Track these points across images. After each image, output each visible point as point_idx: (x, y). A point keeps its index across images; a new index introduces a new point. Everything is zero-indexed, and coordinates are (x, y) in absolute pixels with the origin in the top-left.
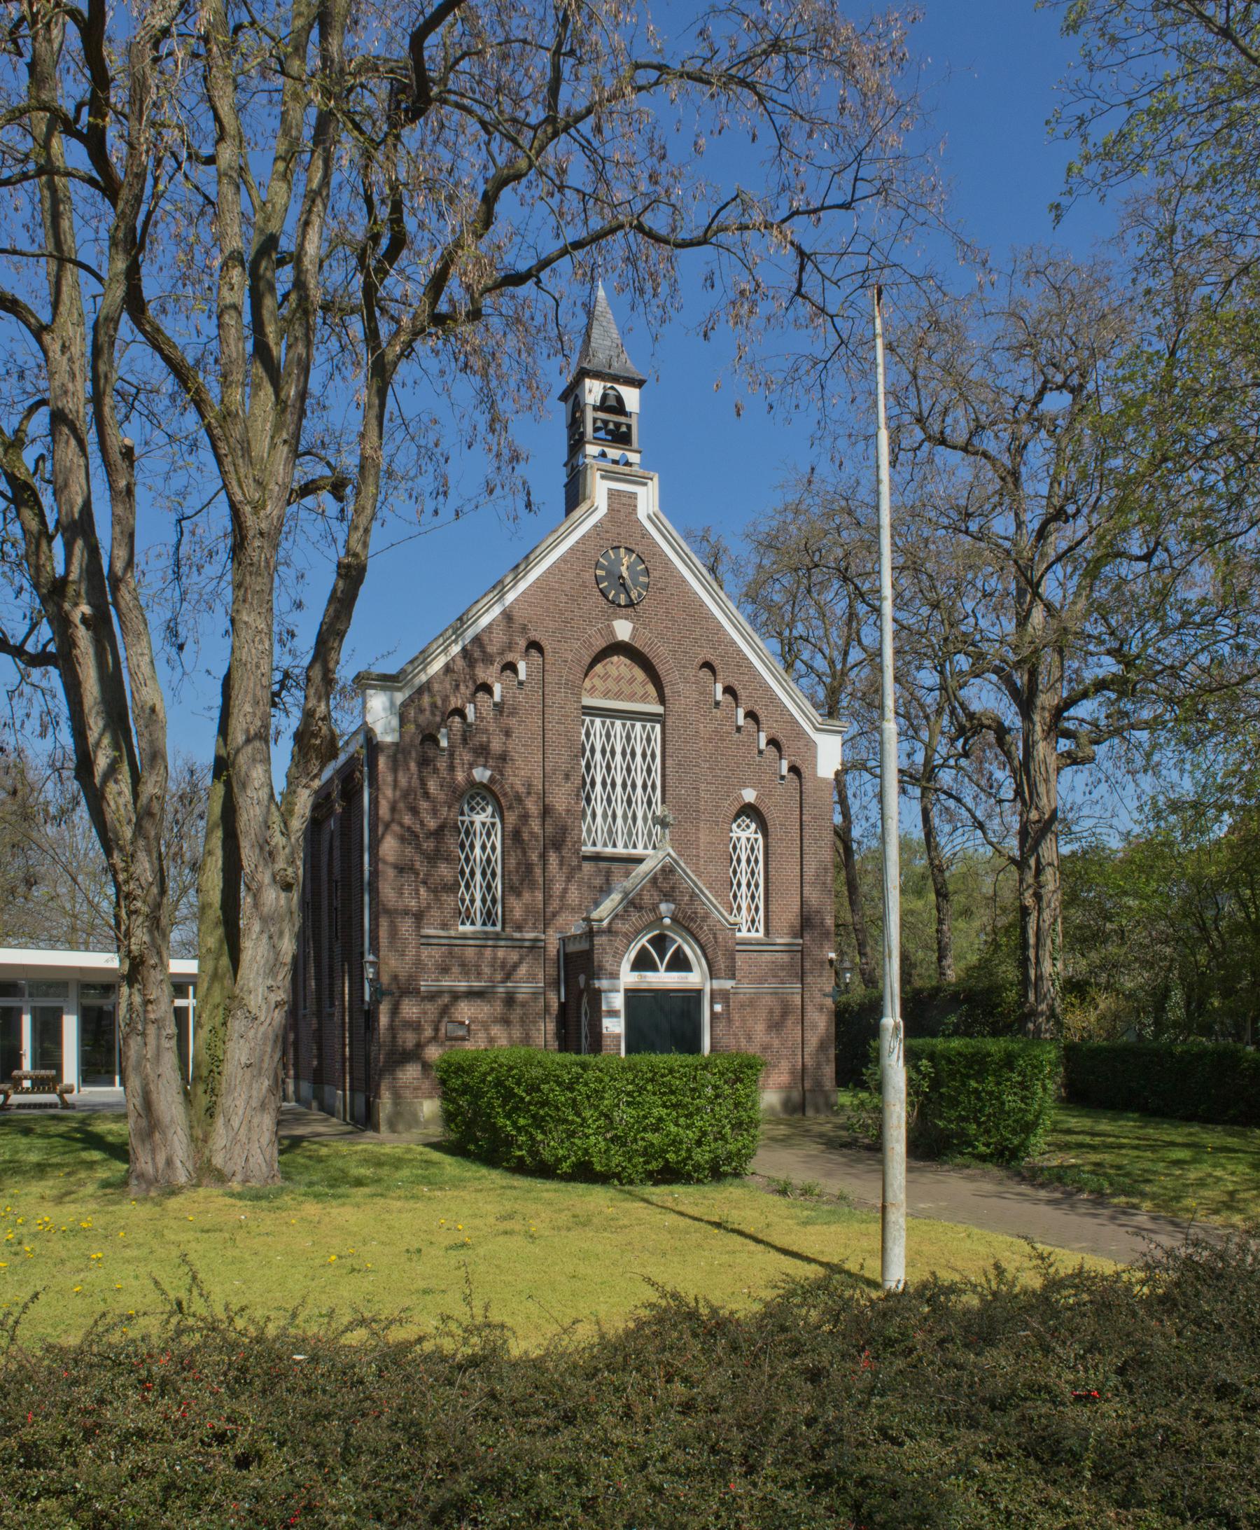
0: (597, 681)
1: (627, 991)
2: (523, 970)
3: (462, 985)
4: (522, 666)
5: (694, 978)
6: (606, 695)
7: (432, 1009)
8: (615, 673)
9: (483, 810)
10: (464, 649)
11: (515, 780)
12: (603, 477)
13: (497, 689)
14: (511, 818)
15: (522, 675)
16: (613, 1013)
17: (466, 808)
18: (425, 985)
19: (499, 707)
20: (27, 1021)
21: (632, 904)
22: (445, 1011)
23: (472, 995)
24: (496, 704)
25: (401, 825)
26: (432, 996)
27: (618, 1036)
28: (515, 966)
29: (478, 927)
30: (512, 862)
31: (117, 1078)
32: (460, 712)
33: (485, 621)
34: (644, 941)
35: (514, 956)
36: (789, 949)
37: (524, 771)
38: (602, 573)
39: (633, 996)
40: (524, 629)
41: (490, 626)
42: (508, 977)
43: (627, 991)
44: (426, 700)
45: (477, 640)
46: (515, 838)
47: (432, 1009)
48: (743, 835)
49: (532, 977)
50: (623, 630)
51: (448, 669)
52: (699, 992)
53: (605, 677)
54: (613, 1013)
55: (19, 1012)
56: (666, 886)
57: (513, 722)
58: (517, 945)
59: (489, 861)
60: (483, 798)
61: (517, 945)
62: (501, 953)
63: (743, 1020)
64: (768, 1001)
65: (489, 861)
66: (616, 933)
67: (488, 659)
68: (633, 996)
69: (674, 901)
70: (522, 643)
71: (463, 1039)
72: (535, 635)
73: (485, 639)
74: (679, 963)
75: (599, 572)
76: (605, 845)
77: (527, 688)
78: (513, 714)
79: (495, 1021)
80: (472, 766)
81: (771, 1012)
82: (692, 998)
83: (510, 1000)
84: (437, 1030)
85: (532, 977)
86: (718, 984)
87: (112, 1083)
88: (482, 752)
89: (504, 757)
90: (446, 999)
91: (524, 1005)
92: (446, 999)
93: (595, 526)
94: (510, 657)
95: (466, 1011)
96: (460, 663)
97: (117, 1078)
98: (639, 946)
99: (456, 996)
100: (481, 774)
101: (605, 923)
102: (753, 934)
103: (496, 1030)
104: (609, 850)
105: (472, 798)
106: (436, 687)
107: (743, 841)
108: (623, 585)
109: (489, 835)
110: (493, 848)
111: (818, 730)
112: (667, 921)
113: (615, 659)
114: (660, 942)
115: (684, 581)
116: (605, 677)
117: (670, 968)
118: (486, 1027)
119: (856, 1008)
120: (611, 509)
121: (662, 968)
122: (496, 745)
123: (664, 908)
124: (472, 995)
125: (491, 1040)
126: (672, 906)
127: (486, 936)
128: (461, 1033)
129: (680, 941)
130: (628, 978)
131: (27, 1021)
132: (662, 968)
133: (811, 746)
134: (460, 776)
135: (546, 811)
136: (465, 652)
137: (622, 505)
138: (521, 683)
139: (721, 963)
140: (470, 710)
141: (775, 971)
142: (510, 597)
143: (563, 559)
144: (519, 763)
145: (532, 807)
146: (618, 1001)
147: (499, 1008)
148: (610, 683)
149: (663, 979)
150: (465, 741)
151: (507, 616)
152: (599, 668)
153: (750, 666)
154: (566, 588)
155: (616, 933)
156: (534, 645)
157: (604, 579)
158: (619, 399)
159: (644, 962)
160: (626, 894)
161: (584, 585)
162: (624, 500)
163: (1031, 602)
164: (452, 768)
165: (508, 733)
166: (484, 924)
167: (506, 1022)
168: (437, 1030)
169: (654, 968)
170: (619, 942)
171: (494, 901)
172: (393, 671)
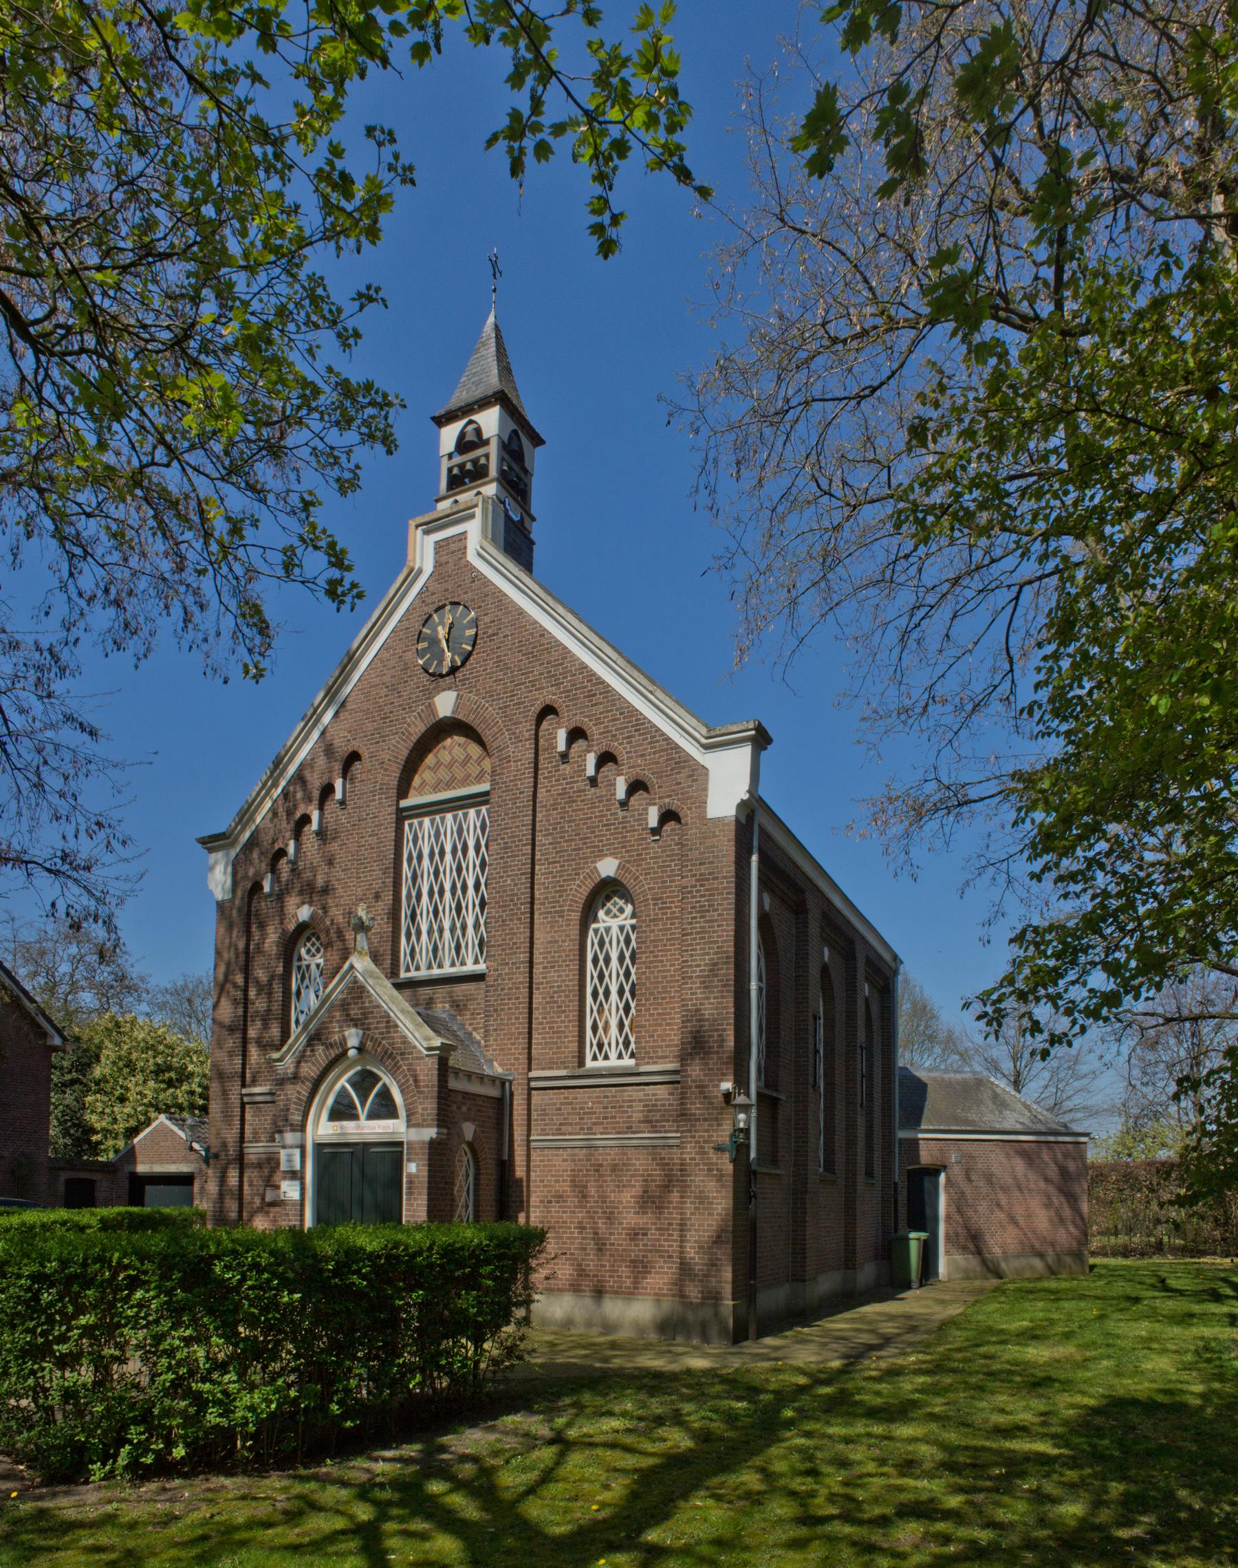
6: (436, 789)
8: (448, 758)
36: (675, 1080)
39: (329, 1155)
48: (614, 924)
50: (445, 704)
51: (274, 812)
53: (434, 769)
56: (355, 1012)
74: (385, 1108)
76: (430, 967)
88: (310, 892)
98: (337, 1087)
104: (436, 972)
107: (615, 931)
111: (707, 747)
114: (365, 1082)
115: (521, 612)
116: (434, 769)
117: (372, 1116)
120: (438, 565)
130: (322, 1129)
133: (699, 774)
137: (450, 552)
152: (430, 759)
153: (607, 689)
154: (385, 679)
159: (343, 1111)
162: (453, 547)
163: (998, 252)
165: (330, 863)
169: (355, 1117)
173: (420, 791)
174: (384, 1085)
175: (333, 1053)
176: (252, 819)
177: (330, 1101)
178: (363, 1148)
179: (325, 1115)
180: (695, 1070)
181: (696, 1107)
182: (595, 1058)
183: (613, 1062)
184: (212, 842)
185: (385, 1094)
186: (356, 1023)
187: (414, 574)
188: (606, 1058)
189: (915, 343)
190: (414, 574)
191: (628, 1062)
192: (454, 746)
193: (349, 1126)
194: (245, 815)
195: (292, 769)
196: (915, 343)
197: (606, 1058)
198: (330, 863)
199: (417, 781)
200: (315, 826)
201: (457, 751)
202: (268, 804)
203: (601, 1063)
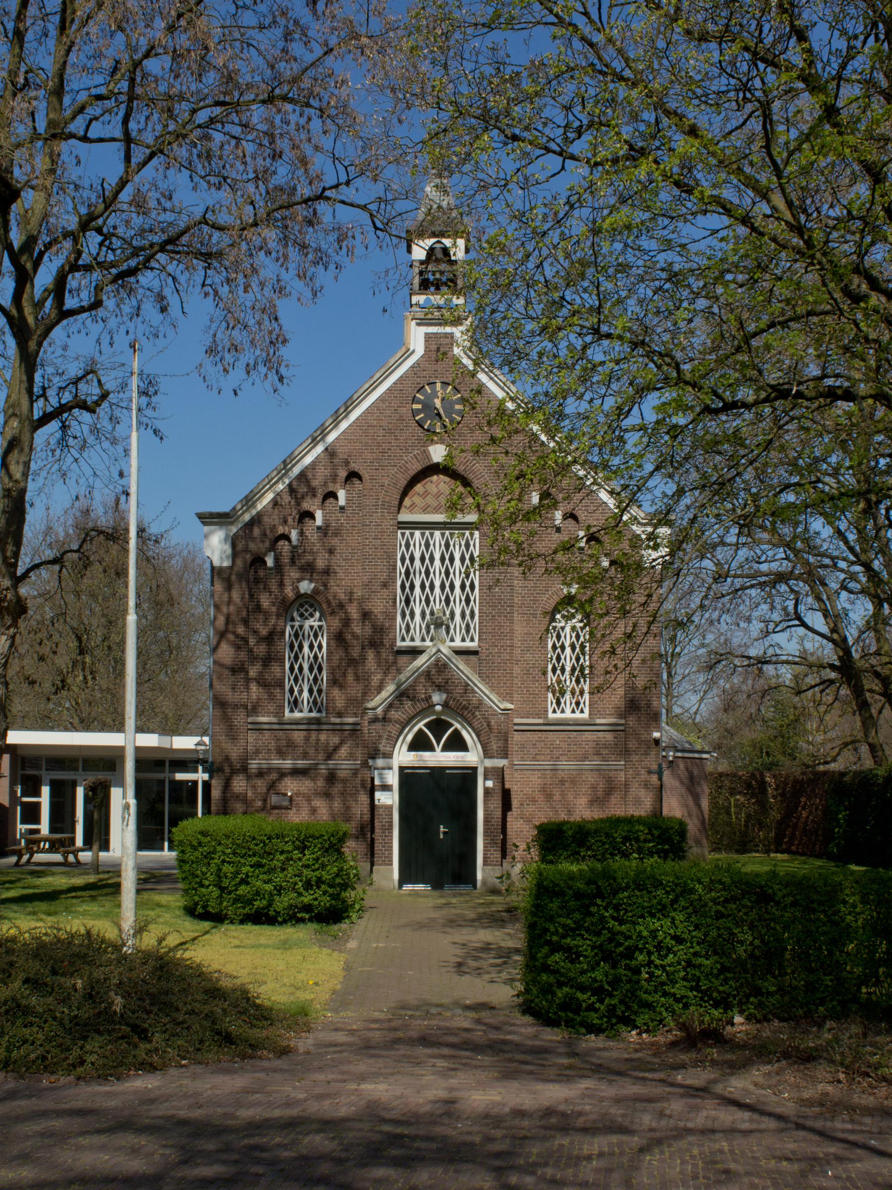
0: (416, 499)
1: (402, 769)
2: (344, 751)
3: (288, 763)
4: (342, 494)
5: (472, 757)
6: (425, 510)
7: (261, 785)
8: (435, 490)
9: (312, 615)
10: (290, 485)
11: (338, 589)
12: (418, 324)
13: (319, 515)
14: (336, 623)
15: (342, 501)
16: (386, 788)
17: (295, 614)
18: (254, 764)
19: (324, 530)
20: (80, 792)
21: (403, 695)
22: (272, 786)
23: (296, 772)
24: (319, 528)
25: (234, 633)
26: (261, 774)
27: (390, 808)
28: (336, 748)
29: (305, 714)
30: (336, 657)
31: (166, 844)
32: (286, 537)
33: (308, 460)
34: (421, 725)
35: (335, 740)
36: (613, 729)
37: (348, 579)
38: (419, 406)
39: (407, 776)
40: (347, 463)
41: (313, 465)
42: (329, 757)
43: (402, 769)
44: (256, 531)
45: (302, 476)
46: (339, 639)
47: (261, 785)
49: (351, 756)
50: (438, 453)
51: (275, 503)
52: (475, 769)
54: (386, 788)
55: (74, 784)
56: (439, 680)
57: (335, 541)
58: (338, 729)
59: (316, 657)
60: (312, 606)
61: (338, 729)
62: (323, 737)
63: (563, 795)
64: (591, 778)
65: (316, 657)
66: (390, 721)
67: (313, 492)
68: (407, 776)
69: (447, 692)
70: (343, 474)
71: (287, 808)
72: (355, 467)
73: (310, 476)
74: (457, 743)
75: (415, 406)
77: (349, 511)
78: (336, 534)
79: (317, 794)
80: (300, 580)
81: (594, 788)
82: (468, 776)
83: (331, 778)
84: (265, 800)
85: (351, 756)
86: (489, 763)
87: (162, 849)
88: (308, 569)
89: (327, 572)
90: (274, 776)
91: (344, 781)
92: (274, 776)
93: (412, 367)
94: (331, 487)
95: (290, 787)
96: (287, 498)
97: (166, 844)
98: (416, 729)
99: (282, 774)
100: (306, 587)
101: (379, 710)
102: (578, 715)
103: (318, 803)
105: (302, 606)
106: (266, 519)
107: (568, 629)
108: (439, 414)
109: (316, 636)
110: (320, 647)
112: (438, 708)
113: (435, 478)
114: (438, 727)
117: (446, 748)
118: (309, 800)
119: (881, 781)
121: (438, 749)
122: (321, 563)
123: (437, 698)
124: (296, 772)
125: (314, 811)
126: (444, 696)
127: (310, 721)
128: (286, 803)
129: (458, 726)
130: (403, 756)
131: (80, 792)
132: (438, 749)
134: (289, 592)
135: (366, 615)
136: (291, 489)
137: (438, 349)
138: (342, 508)
139: (494, 746)
140: (294, 535)
141: (598, 750)
142: (331, 438)
143: (381, 399)
144: (341, 575)
145: (354, 611)
146: (393, 778)
147: (320, 783)
148: (430, 500)
149: (440, 757)
150: (293, 561)
151: (330, 452)
152: (419, 488)
154: (384, 423)
155: (390, 721)
156: (353, 476)
157: (419, 411)
158: (445, 251)
159: (420, 744)
160: (399, 686)
161: (401, 419)
164: (281, 585)
165: (331, 552)
166: (311, 711)
167: (327, 795)
168: (265, 800)
169: (431, 749)
170: (393, 729)
171: (320, 691)
172: (226, 509)
173: (412, 508)
174: (456, 730)
175: (420, 706)
176: (253, 506)
177: (410, 737)
178: (438, 772)
179: (405, 747)
180: (632, 721)
181: (632, 744)
182: (554, 711)
183: (568, 715)
184: (208, 519)
185: (457, 734)
186: (440, 688)
187: (409, 353)
188: (563, 711)
189: (553, 24)
190: (409, 353)
191: (314, 714)
192: (439, 484)
193: (427, 755)
194: (249, 501)
195: (296, 470)
196: (553, 24)
197: (563, 711)
198: (331, 552)
199: (407, 502)
200: (319, 521)
201: (442, 486)
202: (270, 496)
203: (559, 715)
